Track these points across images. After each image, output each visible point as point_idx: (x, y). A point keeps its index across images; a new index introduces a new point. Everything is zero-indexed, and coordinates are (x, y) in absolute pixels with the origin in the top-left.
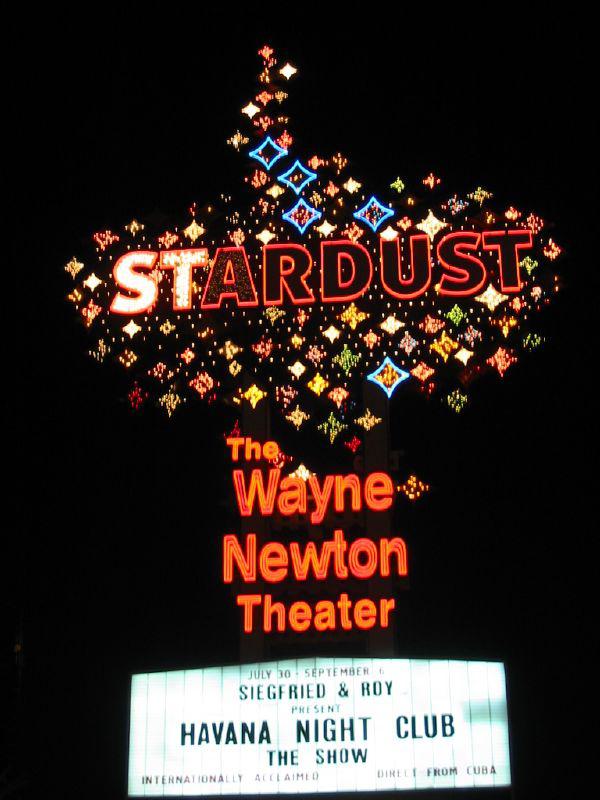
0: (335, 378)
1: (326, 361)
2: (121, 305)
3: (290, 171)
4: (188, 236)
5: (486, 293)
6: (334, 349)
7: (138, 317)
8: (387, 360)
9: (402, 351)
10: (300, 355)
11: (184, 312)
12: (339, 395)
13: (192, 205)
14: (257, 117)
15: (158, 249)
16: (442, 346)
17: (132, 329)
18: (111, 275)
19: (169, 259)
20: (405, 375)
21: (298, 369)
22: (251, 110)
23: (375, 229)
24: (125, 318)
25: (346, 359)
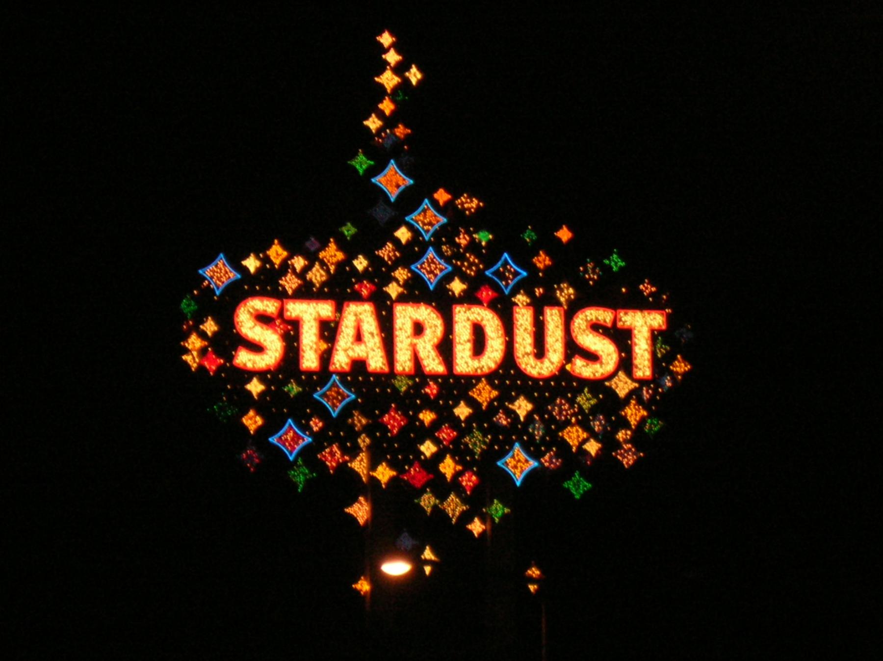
0: (459, 451)
1: (456, 441)
2: (244, 358)
3: (428, 283)
4: (311, 280)
5: (615, 380)
6: (462, 429)
7: (262, 375)
8: (517, 446)
9: (532, 436)
10: (429, 433)
11: (309, 373)
12: (469, 481)
13: (317, 289)
14: (396, 242)
15: (281, 295)
16: (573, 435)
17: (255, 387)
18: (235, 331)
19: (295, 309)
20: (533, 464)
21: (428, 448)
22: (373, 123)
23: (507, 292)
24: (248, 375)
25: (477, 442)
